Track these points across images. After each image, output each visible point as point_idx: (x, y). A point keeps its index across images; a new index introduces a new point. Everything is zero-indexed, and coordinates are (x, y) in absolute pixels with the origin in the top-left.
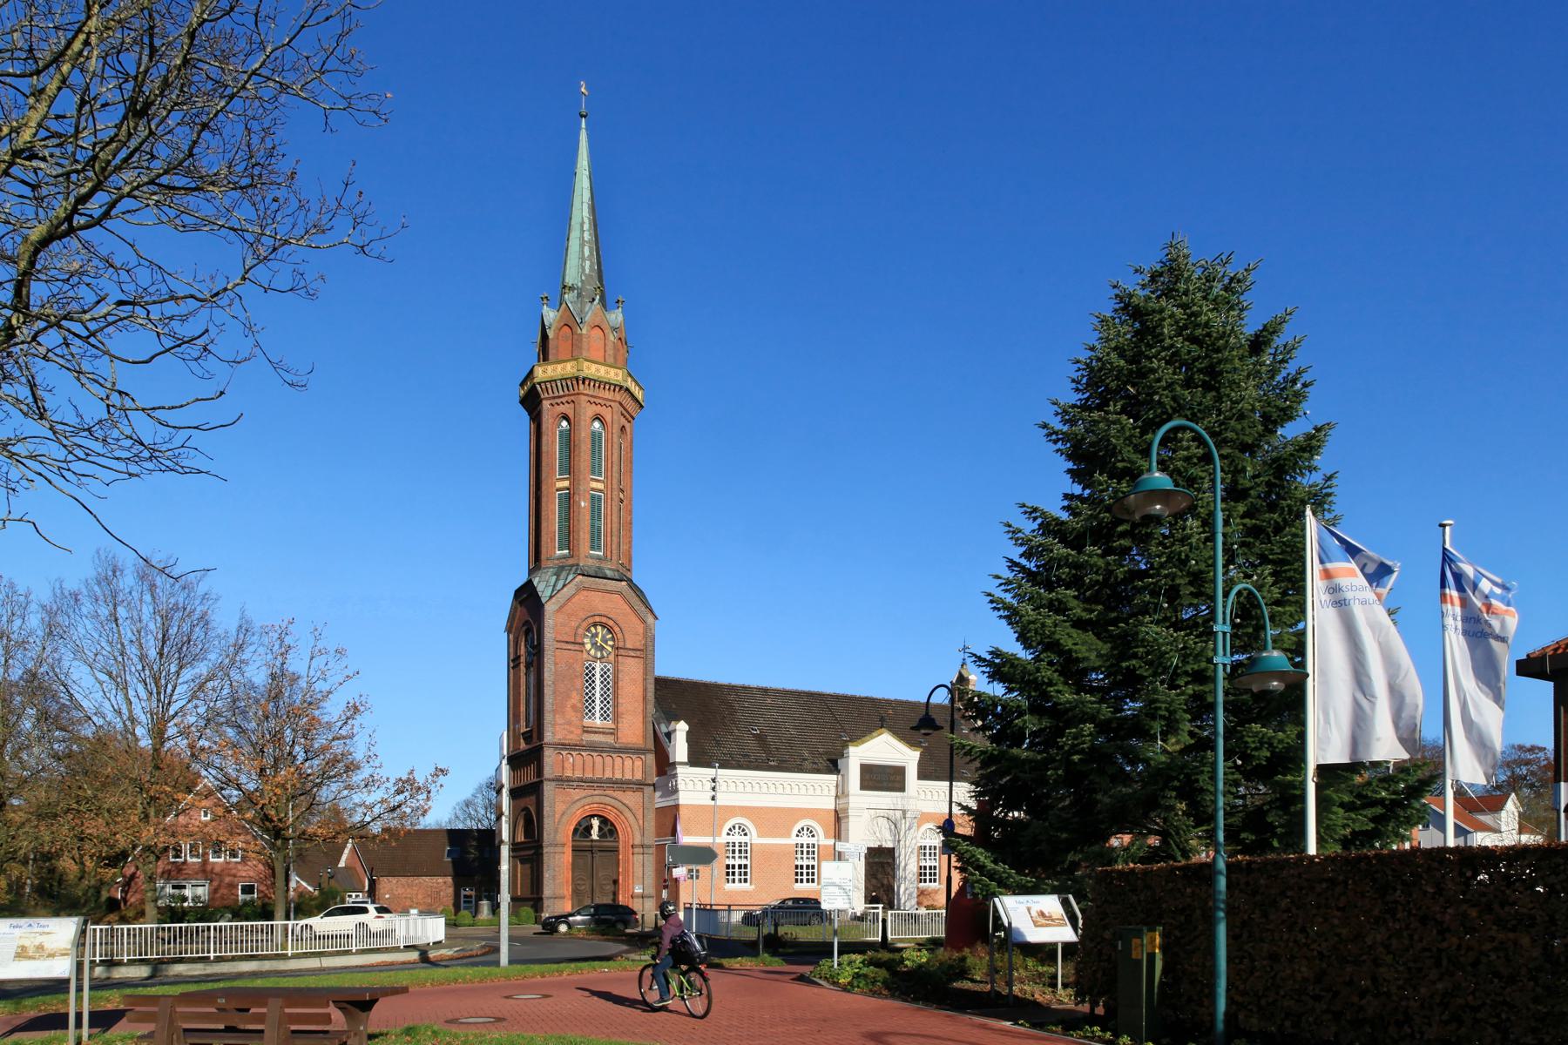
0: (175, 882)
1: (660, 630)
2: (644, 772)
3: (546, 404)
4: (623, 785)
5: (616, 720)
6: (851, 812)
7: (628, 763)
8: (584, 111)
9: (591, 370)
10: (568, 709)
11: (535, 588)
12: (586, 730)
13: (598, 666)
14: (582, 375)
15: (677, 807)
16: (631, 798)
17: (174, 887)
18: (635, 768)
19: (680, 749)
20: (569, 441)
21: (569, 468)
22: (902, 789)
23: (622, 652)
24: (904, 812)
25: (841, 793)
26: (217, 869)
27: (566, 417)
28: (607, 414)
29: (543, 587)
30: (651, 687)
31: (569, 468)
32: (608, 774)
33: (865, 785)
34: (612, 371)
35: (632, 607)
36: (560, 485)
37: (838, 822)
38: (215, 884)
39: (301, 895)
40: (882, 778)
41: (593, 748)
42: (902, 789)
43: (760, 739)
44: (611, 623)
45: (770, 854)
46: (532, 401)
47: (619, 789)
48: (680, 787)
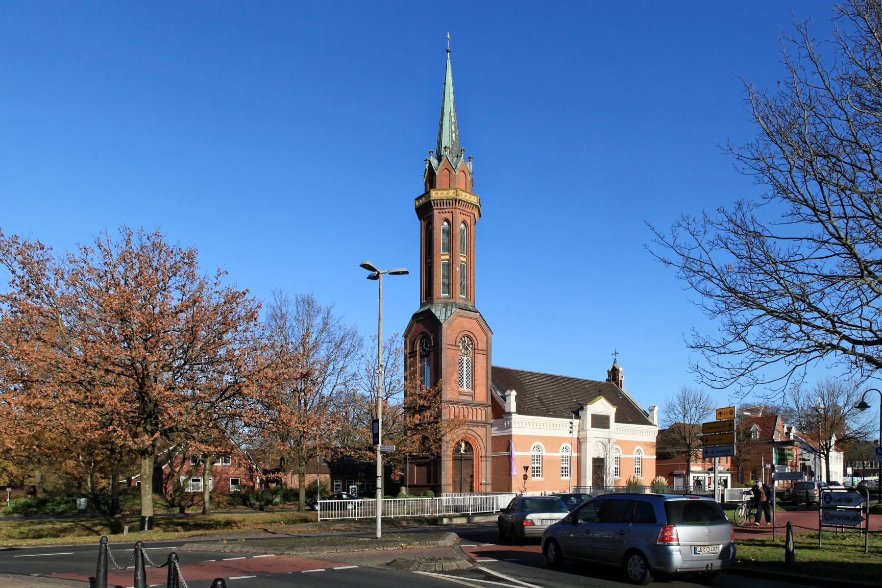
0: (195, 478)
1: (494, 339)
2: (486, 417)
3: (436, 212)
4: (476, 424)
5: (473, 388)
6: (588, 439)
8: (449, 49)
9: (463, 196)
10: (453, 382)
11: (434, 315)
12: (461, 394)
13: (465, 358)
14: (459, 198)
15: (510, 436)
16: (481, 431)
17: (194, 480)
18: (482, 414)
19: (512, 404)
20: (449, 233)
21: (449, 248)
22: (608, 427)
24: (609, 440)
25: (581, 429)
26: (219, 470)
27: (447, 220)
28: (468, 220)
29: (439, 312)
30: (490, 371)
31: (449, 248)
33: (593, 426)
34: (473, 197)
35: (481, 327)
36: (443, 257)
37: (580, 443)
38: (218, 478)
40: (600, 422)
41: (464, 403)
42: (608, 427)
43: (539, 399)
45: (552, 460)
46: (425, 211)
48: (513, 425)
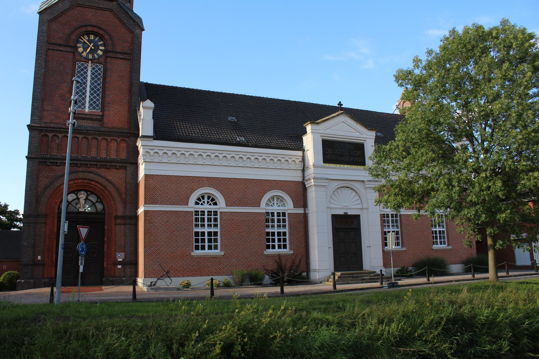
7: (113, 145)
23: (111, 54)
32: (93, 154)
35: (121, 21)
39: (499, 220)
44: (101, 32)
47: (102, 167)
